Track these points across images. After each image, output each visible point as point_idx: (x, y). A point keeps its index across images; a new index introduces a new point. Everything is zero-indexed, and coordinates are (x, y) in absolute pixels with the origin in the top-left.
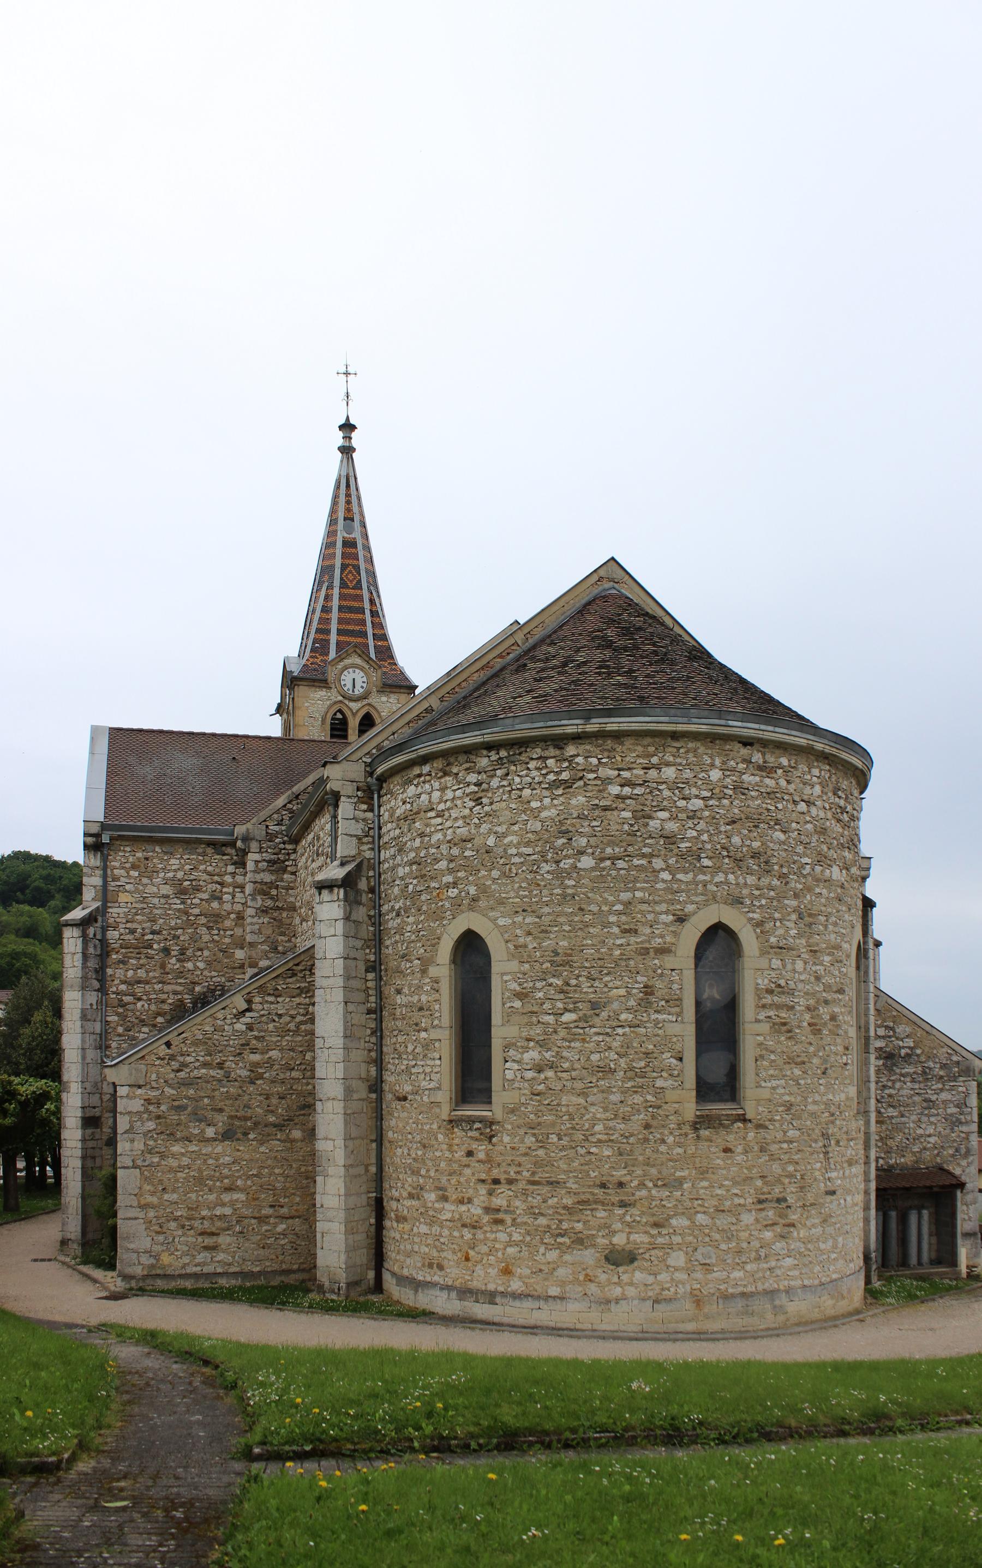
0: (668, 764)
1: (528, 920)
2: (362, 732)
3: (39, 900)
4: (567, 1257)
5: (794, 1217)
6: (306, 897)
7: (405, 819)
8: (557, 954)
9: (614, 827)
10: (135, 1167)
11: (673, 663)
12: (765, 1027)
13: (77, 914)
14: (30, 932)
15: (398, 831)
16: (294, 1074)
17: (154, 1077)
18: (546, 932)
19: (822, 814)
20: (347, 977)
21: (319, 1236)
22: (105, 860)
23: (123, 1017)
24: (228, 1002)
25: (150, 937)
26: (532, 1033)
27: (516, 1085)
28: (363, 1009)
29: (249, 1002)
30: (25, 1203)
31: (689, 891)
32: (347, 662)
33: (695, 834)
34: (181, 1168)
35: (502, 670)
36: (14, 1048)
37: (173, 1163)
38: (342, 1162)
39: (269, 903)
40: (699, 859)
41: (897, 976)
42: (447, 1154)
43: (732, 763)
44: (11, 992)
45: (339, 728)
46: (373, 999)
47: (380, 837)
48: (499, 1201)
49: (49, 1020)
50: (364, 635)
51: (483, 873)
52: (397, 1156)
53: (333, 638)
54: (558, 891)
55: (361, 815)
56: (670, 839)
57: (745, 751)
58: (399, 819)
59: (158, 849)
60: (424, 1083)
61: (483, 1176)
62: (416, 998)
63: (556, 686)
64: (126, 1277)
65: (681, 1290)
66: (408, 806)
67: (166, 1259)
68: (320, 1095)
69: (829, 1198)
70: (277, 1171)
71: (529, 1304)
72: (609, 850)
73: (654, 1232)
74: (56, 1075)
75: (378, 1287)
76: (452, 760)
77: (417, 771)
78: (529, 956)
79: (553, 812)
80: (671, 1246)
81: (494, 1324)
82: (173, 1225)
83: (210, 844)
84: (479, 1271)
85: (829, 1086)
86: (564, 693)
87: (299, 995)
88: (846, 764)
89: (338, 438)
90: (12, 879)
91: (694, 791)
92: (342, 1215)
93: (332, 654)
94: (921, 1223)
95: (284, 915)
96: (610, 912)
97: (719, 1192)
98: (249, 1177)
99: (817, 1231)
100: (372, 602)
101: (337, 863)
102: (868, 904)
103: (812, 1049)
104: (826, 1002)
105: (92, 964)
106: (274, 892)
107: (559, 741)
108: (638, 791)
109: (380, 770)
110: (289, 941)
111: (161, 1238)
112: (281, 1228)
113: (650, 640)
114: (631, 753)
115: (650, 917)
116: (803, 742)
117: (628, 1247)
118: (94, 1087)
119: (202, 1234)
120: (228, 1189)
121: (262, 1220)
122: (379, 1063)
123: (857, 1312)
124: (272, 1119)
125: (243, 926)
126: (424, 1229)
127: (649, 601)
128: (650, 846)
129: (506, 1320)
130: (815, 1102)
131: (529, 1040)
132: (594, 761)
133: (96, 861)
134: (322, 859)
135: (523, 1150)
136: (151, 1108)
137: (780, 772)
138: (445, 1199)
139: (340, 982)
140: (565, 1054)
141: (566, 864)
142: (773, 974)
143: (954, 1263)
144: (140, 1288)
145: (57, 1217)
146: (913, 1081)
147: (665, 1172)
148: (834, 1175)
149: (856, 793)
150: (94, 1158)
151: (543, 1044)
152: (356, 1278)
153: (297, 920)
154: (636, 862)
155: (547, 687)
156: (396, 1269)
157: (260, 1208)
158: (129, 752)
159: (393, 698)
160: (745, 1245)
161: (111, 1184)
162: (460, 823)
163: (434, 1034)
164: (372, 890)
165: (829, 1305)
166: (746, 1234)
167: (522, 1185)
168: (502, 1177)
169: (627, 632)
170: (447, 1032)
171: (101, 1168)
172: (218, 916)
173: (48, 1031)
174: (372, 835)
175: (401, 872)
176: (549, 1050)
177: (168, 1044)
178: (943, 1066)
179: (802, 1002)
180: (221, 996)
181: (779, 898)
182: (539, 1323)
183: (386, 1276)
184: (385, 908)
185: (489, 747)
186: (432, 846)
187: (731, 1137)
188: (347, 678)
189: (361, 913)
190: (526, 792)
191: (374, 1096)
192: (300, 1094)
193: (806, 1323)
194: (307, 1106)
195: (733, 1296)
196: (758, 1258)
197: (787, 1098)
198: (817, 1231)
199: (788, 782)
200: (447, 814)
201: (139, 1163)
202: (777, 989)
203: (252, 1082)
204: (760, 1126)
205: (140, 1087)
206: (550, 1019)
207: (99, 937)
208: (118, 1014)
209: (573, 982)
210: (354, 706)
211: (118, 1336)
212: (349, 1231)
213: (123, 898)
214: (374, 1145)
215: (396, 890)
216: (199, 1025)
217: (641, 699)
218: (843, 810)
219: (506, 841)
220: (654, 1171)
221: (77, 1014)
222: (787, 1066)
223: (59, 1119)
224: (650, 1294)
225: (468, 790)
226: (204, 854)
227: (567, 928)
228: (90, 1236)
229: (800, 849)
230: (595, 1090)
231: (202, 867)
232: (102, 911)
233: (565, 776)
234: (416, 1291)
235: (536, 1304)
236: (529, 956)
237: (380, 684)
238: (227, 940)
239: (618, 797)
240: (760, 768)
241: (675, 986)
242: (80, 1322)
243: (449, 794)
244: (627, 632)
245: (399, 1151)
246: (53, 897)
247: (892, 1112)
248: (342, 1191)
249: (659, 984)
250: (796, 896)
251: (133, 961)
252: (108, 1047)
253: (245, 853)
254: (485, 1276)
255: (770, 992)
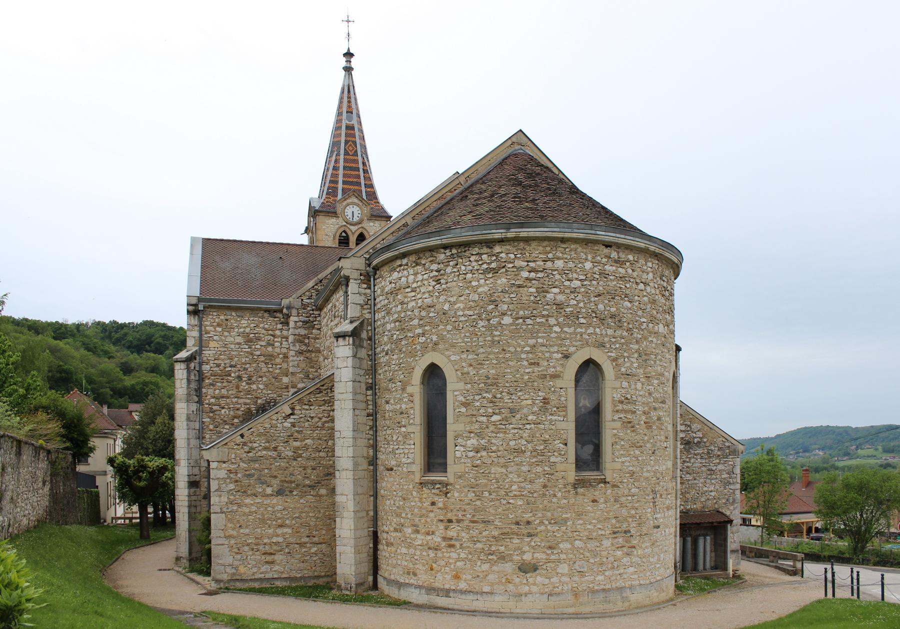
0: (559, 258)
1: (470, 357)
2: (357, 244)
3: (159, 350)
4: (494, 568)
5: (635, 542)
6: (327, 344)
7: (391, 293)
8: (489, 378)
9: (524, 298)
10: (222, 512)
11: (560, 195)
12: (618, 424)
13: (183, 354)
14: (154, 370)
15: (386, 301)
16: (322, 454)
17: (233, 456)
18: (481, 364)
19: (653, 291)
20: (355, 393)
21: (338, 555)
22: (200, 320)
23: (213, 419)
24: (279, 409)
25: (229, 369)
26: (473, 428)
27: (463, 461)
28: (365, 413)
29: (293, 409)
30: (153, 534)
31: (571, 339)
32: (349, 201)
33: (575, 302)
34: (251, 513)
35: (451, 200)
36: (145, 439)
37: (247, 510)
38: (352, 509)
39: (304, 348)
40: (578, 318)
41: (685, 395)
42: (419, 504)
43: (599, 258)
44: (142, 405)
45: (344, 241)
46: (370, 407)
47: (375, 305)
48: (451, 533)
49: (166, 422)
50: (359, 184)
51: (441, 327)
52: (387, 505)
53: (340, 186)
54: (489, 338)
55: (363, 291)
56: (559, 306)
57: (606, 251)
58: (387, 293)
59: (234, 314)
60: (403, 460)
61: (442, 518)
62: (399, 406)
63: (487, 209)
64: (218, 581)
65: (566, 588)
66: (393, 285)
67: (242, 569)
68: (337, 467)
69: (656, 530)
70: (311, 515)
71: (471, 597)
72: (521, 313)
73: (549, 552)
74: (171, 456)
75: (375, 586)
76: (421, 255)
77: (399, 262)
78: (471, 380)
79: (486, 289)
80: (559, 561)
81: (449, 609)
82: (246, 548)
83: (266, 311)
84: (439, 576)
85: (656, 461)
86: (492, 213)
87: (324, 405)
88: (667, 259)
89: (343, 62)
90: (143, 338)
91: (575, 275)
92: (352, 542)
93: (340, 196)
94: (705, 544)
95: (313, 355)
96: (522, 352)
97: (589, 527)
98: (293, 519)
99: (649, 550)
100: (364, 164)
101: (348, 321)
102: (678, 349)
103: (646, 438)
104: (655, 409)
105: (193, 385)
106: (307, 341)
107: (490, 243)
108: (540, 275)
109: (374, 263)
110: (316, 371)
111: (239, 557)
112: (314, 550)
113: (545, 180)
114: (536, 251)
115: (547, 355)
116: (642, 245)
117: (533, 562)
118: (195, 463)
119: (264, 554)
120: (281, 526)
121: (302, 545)
122: (375, 447)
123: (672, 600)
124: (307, 482)
125: (287, 362)
126: (404, 550)
127: (544, 158)
128: (547, 310)
129: (456, 607)
130: (648, 471)
131: (470, 432)
132: (512, 256)
133: (194, 321)
134: (337, 319)
135: (467, 501)
136: (232, 475)
137: (628, 264)
138: (418, 532)
139: (350, 396)
140: (493, 441)
141: (494, 321)
142: (623, 391)
143: (725, 569)
144: (226, 588)
145: (173, 542)
146: (702, 458)
147: (556, 515)
148: (658, 516)
149: (673, 278)
150: (196, 506)
151: (479, 435)
152: (361, 581)
153: (321, 359)
154: (538, 320)
155: (481, 210)
156: (386, 575)
157: (301, 537)
158: (214, 253)
159: (377, 224)
160: (605, 560)
161: (207, 523)
162: (427, 295)
163: (410, 429)
164: (370, 339)
165: (656, 596)
166: (606, 553)
167: (466, 523)
168: (454, 518)
169: (530, 176)
170: (419, 428)
171: (200, 513)
172: (272, 356)
173: (166, 428)
174: (370, 304)
175: (388, 327)
176: (483, 438)
177: (242, 436)
178: (720, 449)
179: (640, 409)
180: (274, 406)
181: (627, 344)
182: (477, 609)
183: (380, 580)
184: (378, 350)
185: (445, 247)
186: (408, 310)
187: (596, 493)
188: (349, 211)
189: (363, 353)
190: (469, 276)
191: (372, 468)
192: (325, 466)
193: (641, 607)
194: (330, 473)
195: (598, 591)
196: (613, 568)
197: (631, 468)
198: (649, 550)
199: (633, 271)
200: (418, 290)
201: (225, 510)
202: (625, 400)
203: (295, 459)
204: (614, 486)
205: (224, 462)
206: (484, 419)
207: (197, 369)
208: (209, 417)
209: (499, 396)
210: (353, 228)
211: (214, 620)
212: (357, 552)
213: (212, 344)
214: (372, 498)
215: (385, 338)
216: (261, 423)
217: (542, 217)
218: (666, 289)
219: (456, 307)
220: (549, 514)
221: (184, 417)
222: (631, 449)
223: (174, 482)
224: (546, 590)
225: (432, 275)
226: (263, 317)
227: (495, 362)
228: (194, 555)
229: (640, 313)
230: (512, 464)
231: (261, 325)
232: (199, 352)
233: (493, 265)
234: (399, 589)
235: (475, 597)
236: (471, 380)
237: (369, 215)
238: (278, 371)
239: (527, 279)
240: (616, 262)
241: (563, 399)
242: (189, 610)
243: (420, 277)
244: (530, 176)
245: (388, 502)
246: (168, 348)
247: (688, 477)
248: (352, 527)
249: (552, 397)
250: (637, 342)
251: (219, 384)
252: (204, 438)
253: (288, 316)
254: (444, 580)
255: (621, 402)
